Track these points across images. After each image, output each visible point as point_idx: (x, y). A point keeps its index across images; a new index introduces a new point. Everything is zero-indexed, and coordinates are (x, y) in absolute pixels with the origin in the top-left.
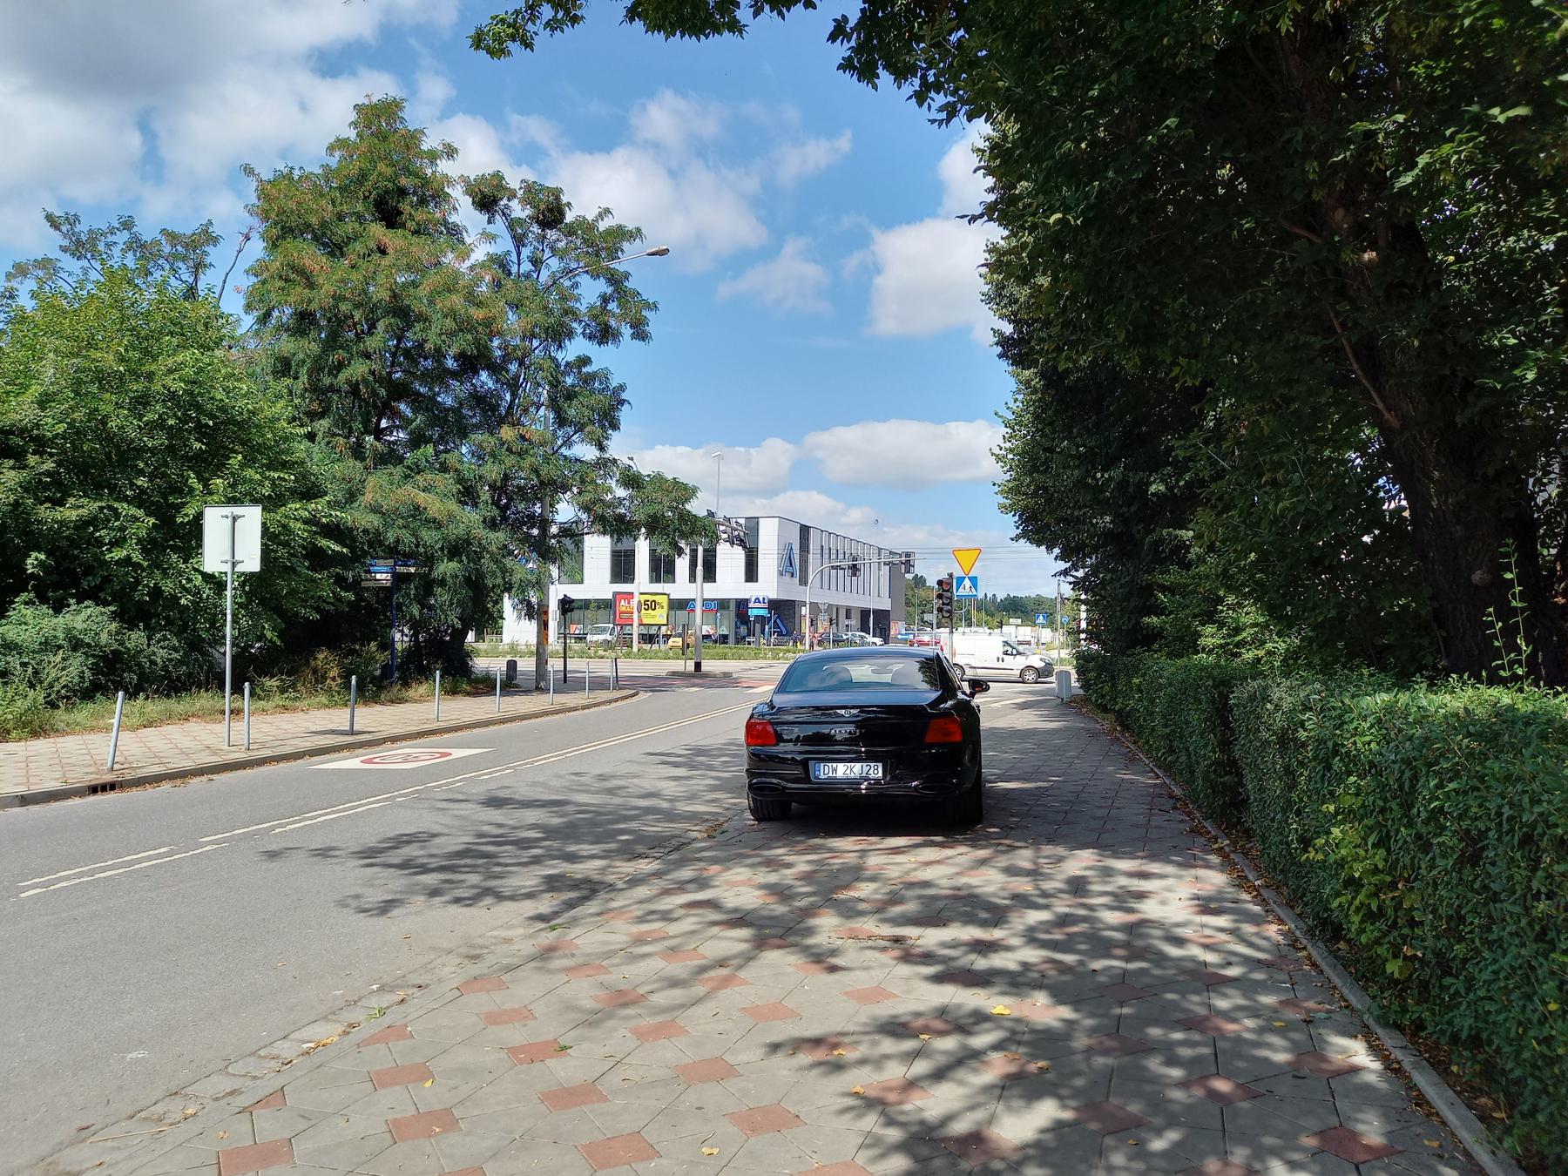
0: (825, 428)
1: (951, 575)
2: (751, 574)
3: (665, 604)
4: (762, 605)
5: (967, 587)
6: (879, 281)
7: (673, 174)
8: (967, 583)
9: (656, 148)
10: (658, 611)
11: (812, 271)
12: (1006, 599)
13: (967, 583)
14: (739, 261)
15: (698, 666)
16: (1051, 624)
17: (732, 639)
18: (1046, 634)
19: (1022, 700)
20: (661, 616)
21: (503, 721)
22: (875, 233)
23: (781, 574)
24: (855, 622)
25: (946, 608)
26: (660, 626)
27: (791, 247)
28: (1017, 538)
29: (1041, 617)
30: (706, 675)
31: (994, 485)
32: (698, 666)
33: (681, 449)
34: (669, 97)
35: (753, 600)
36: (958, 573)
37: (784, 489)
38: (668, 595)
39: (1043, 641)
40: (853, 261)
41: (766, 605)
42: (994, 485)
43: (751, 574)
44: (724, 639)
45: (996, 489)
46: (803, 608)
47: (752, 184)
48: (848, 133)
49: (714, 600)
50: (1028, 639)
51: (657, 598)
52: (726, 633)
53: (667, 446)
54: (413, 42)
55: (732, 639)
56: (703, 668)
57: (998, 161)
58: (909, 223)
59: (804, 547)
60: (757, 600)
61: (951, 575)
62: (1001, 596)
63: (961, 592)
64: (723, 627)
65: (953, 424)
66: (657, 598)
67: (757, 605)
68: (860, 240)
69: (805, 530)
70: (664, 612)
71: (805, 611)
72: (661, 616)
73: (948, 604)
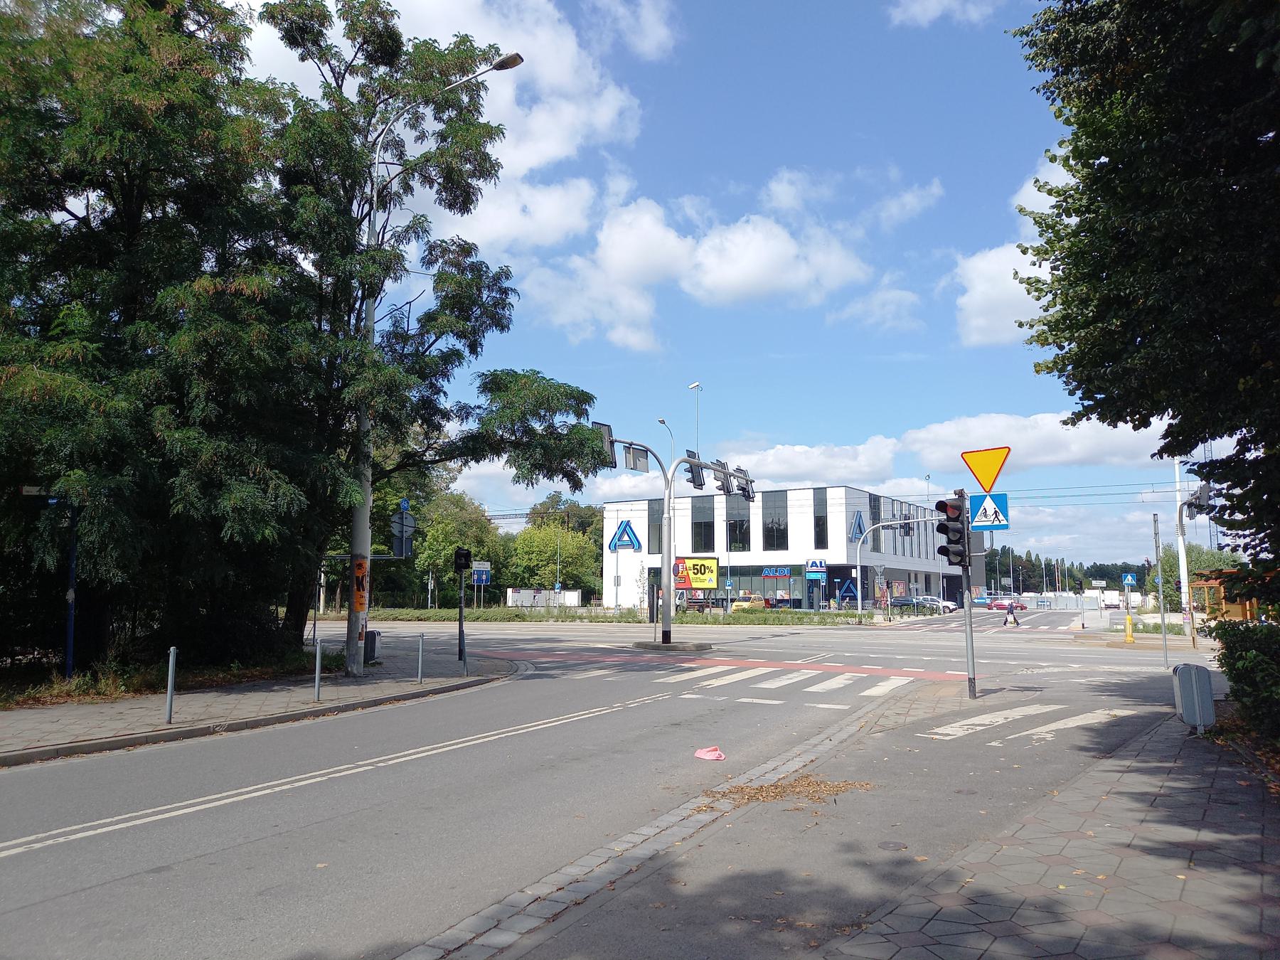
0: (920, 426)
1: (960, 494)
2: (821, 540)
3: (714, 568)
4: (819, 569)
5: (990, 512)
6: (962, 301)
7: (794, 234)
8: (989, 505)
9: (780, 218)
10: (708, 575)
11: (909, 297)
12: (1092, 567)
13: (989, 505)
14: (851, 292)
15: (666, 635)
16: (1140, 586)
17: (805, 603)
18: (1136, 598)
19: (1098, 717)
20: (711, 580)
21: (316, 714)
22: (959, 258)
23: (851, 540)
24: (921, 585)
25: (953, 547)
26: (710, 590)
27: (886, 279)
28: (1075, 419)
29: (1129, 577)
30: (674, 649)
31: (1021, 325)
32: (666, 635)
33: (798, 448)
34: (786, 175)
35: (810, 564)
36: (972, 489)
37: (890, 478)
38: (718, 559)
39: (1133, 604)
40: (943, 282)
41: (824, 569)
42: (1021, 325)
43: (821, 540)
44: (797, 604)
45: (1027, 332)
46: (854, 571)
47: (859, 233)
48: (936, 181)
49: (787, 566)
50: (1116, 603)
51: (707, 563)
52: (799, 597)
53: (787, 446)
54: (604, 153)
55: (805, 603)
56: (675, 637)
57: (1074, 221)
58: (991, 248)
59: (875, 517)
60: (814, 564)
61: (960, 494)
62: (1087, 565)
63: (979, 521)
64: (797, 592)
65: (1039, 416)
66: (707, 563)
67: (814, 569)
68: (951, 266)
69: (875, 501)
70: (714, 576)
71: (855, 573)
72: (711, 580)
73: (957, 542)
